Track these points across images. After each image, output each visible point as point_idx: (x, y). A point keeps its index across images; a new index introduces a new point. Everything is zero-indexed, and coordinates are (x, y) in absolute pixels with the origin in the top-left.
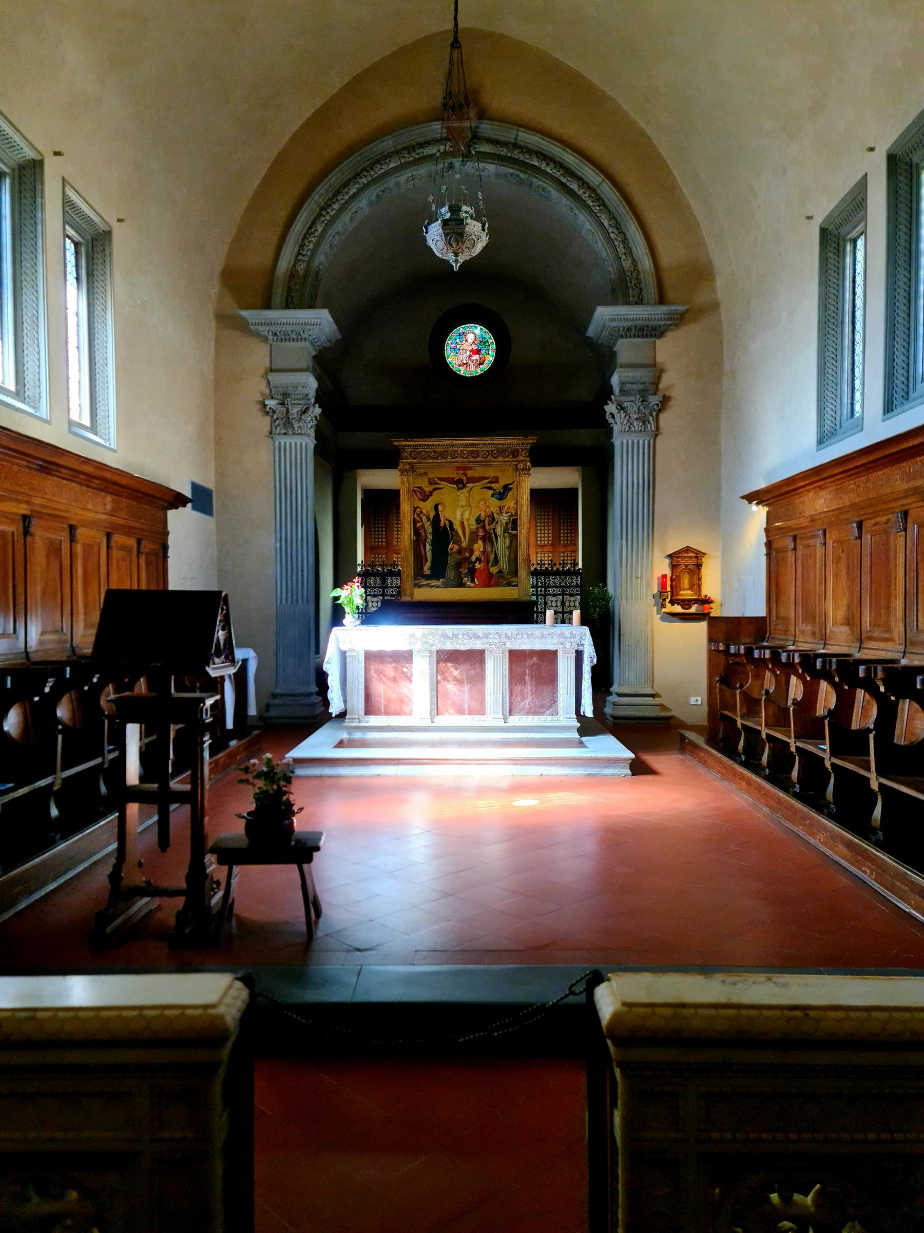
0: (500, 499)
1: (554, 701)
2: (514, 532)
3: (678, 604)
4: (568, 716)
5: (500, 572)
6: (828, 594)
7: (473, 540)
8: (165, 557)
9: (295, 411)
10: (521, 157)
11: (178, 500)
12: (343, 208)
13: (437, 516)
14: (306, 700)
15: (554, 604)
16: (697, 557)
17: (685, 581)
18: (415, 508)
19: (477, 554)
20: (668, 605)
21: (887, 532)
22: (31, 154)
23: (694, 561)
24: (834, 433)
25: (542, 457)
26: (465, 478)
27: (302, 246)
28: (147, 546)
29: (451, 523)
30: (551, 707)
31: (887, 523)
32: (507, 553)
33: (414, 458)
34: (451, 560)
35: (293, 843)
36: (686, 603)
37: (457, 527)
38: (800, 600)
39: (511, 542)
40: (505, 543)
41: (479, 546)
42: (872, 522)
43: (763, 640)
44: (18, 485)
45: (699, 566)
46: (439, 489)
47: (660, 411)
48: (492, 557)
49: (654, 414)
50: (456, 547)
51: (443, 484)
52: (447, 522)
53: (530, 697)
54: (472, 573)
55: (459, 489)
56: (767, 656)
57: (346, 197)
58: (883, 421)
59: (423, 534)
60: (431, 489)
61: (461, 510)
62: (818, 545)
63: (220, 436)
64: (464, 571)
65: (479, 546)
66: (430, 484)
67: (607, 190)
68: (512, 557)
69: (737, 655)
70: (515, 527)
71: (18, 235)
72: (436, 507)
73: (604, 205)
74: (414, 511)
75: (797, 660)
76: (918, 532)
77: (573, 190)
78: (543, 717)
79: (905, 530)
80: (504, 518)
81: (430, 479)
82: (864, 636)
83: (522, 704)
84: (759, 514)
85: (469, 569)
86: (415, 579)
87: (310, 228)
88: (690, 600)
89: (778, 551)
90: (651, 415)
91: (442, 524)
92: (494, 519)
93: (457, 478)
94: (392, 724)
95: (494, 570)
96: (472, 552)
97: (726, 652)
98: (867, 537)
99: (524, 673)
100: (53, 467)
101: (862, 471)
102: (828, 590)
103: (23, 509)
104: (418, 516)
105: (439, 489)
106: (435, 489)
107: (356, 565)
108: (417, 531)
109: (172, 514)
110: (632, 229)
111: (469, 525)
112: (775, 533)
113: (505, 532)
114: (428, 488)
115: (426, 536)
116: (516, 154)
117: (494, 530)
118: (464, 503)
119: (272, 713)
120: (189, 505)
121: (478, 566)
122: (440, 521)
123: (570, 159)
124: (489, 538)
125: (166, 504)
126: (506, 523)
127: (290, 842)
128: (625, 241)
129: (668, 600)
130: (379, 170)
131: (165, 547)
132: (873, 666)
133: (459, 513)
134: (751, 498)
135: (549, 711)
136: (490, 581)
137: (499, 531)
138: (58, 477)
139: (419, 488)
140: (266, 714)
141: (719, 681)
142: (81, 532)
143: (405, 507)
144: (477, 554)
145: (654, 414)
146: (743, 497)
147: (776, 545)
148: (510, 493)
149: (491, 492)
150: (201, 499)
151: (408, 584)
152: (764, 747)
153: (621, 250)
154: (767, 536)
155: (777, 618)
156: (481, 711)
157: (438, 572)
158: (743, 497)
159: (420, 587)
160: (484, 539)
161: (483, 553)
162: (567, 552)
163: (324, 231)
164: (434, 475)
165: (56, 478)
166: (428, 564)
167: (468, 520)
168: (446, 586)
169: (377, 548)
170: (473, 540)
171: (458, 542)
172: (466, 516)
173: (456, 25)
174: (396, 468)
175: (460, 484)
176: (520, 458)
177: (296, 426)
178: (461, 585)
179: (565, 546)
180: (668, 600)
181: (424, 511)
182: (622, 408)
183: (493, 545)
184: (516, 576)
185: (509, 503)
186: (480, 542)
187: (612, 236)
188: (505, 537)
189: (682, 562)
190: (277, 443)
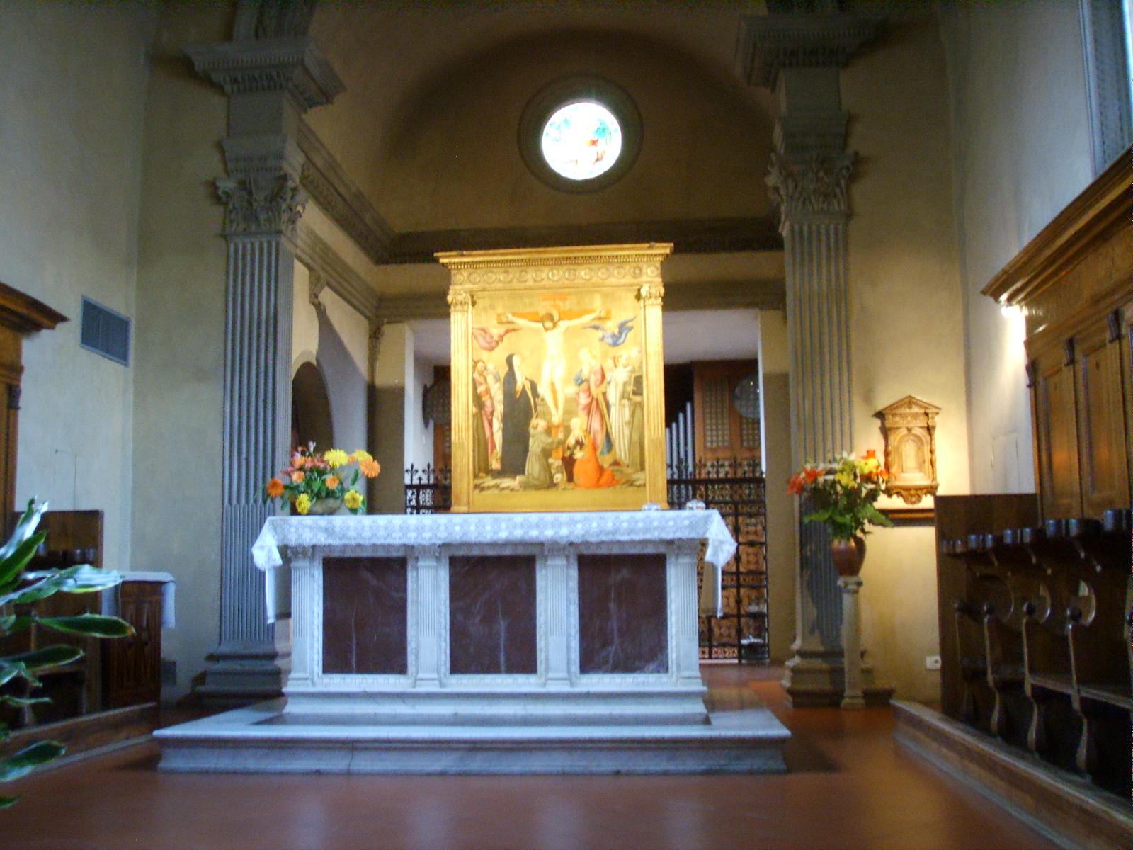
2: (638, 399)
4: (686, 674)
7: (569, 413)
9: (260, 196)
13: (510, 377)
16: (926, 414)
23: (922, 422)
29: (534, 387)
32: (627, 432)
33: (474, 284)
34: (535, 445)
36: (912, 492)
37: (543, 390)
39: (633, 415)
40: (623, 416)
45: (930, 430)
46: (514, 330)
48: (600, 439)
49: (843, 182)
51: (521, 322)
53: (617, 641)
54: (569, 463)
55: (546, 329)
56: (1027, 539)
59: (488, 403)
64: (556, 462)
66: (500, 323)
68: (636, 437)
70: (638, 391)
72: (509, 361)
74: (474, 368)
75: (1074, 530)
83: (604, 653)
85: (563, 459)
86: (476, 476)
90: (838, 185)
91: (519, 387)
92: (603, 377)
93: (542, 312)
94: (370, 689)
95: (606, 461)
96: (568, 431)
104: (481, 374)
105: (514, 330)
106: (507, 332)
113: (623, 397)
114: (496, 331)
115: (493, 406)
117: (604, 394)
121: (579, 455)
124: (598, 407)
126: (625, 384)
135: (652, 666)
137: (613, 397)
140: (200, 688)
141: (961, 609)
145: (843, 182)
148: (630, 334)
156: (525, 662)
158: (984, 293)
159: (483, 489)
161: (588, 431)
168: (526, 486)
171: (546, 415)
173: (1081, 489)
177: (262, 217)
178: (552, 485)
181: (490, 367)
185: (628, 352)
188: (622, 406)
190: (232, 247)
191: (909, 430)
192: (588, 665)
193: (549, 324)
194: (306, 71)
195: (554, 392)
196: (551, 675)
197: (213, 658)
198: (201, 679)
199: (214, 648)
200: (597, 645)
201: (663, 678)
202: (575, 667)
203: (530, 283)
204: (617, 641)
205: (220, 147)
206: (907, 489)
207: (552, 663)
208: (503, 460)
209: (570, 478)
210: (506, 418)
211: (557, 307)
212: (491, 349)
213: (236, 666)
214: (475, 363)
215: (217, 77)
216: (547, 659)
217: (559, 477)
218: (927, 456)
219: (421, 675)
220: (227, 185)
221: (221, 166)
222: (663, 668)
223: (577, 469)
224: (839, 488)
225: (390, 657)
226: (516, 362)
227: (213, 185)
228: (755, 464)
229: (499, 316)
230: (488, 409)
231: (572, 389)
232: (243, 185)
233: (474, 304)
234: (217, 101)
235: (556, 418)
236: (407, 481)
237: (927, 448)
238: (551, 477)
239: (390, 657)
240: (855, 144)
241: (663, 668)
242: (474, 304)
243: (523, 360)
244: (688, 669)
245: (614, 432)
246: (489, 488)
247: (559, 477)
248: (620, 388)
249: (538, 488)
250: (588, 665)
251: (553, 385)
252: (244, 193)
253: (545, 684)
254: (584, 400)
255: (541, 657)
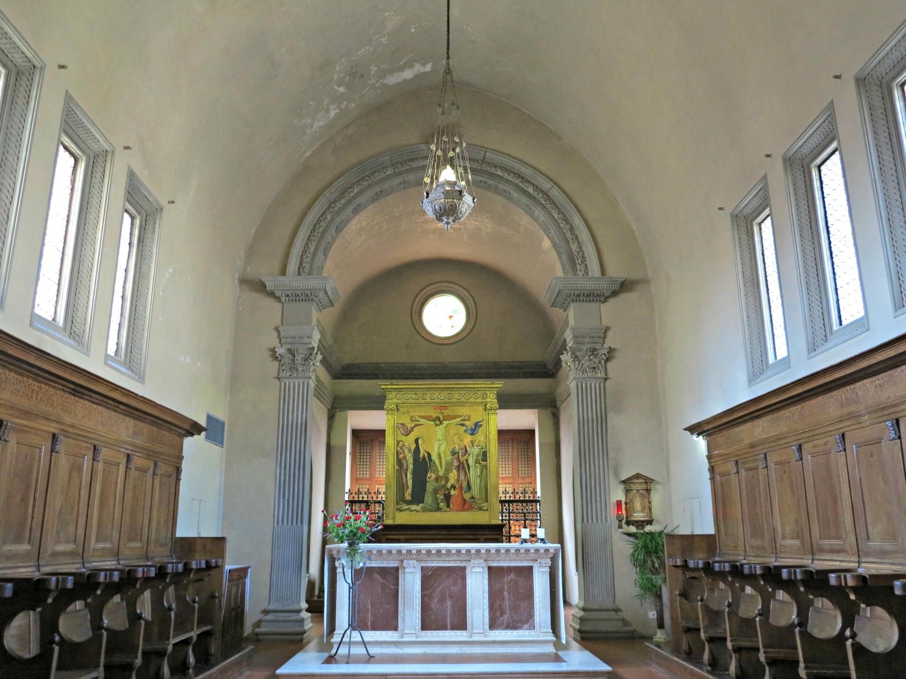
0: (472, 434)
1: (531, 616)
2: (484, 463)
3: (633, 525)
4: (544, 630)
5: (473, 498)
6: (774, 511)
7: (448, 470)
8: (178, 479)
9: (299, 358)
10: (488, 169)
11: (194, 429)
12: (349, 202)
13: (417, 449)
14: (294, 617)
15: (517, 528)
17: (638, 504)
18: (398, 442)
19: (452, 481)
20: (624, 526)
21: (827, 453)
22: (106, 146)
23: (644, 486)
24: (762, 371)
25: (506, 401)
26: (441, 417)
27: (313, 230)
28: (163, 468)
29: (429, 455)
30: (527, 622)
31: (825, 445)
32: (478, 481)
34: (430, 487)
35: (811, 597)
37: (434, 457)
38: (747, 519)
39: (481, 472)
41: (453, 476)
42: (811, 444)
43: (714, 556)
44: (52, 406)
45: (648, 491)
47: (607, 360)
48: (465, 484)
50: (434, 476)
51: (423, 421)
52: (426, 455)
53: (508, 612)
54: (448, 498)
55: (437, 425)
57: (352, 195)
58: (809, 359)
60: (412, 425)
61: (438, 444)
62: (760, 467)
63: (235, 381)
64: (440, 497)
65: (453, 476)
67: (555, 193)
68: (483, 484)
69: (696, 569)
70: (485, 458)
71: (84, 213)
72: (417, 441)
73: (554, 204)
75: (759, 572)
76: (857, 451)
77: (529, 193)
78: (520, 632)
79: (845, 450)
80: (476, 451)
81: (411, 417)
82: (815, 547)
83: (501, 619)
84: (701, 443)
86: (397, 504)
87: (322, 216)
88: (643, 522)
89: (723, 475)
92: (466, 451)
93: (435, 415)
95: (467, 496)
96: (447, 480)
97: (685, 566)
98: (807, 458)
99: (503, 589)
100: (86, 392)
101: (796, 402)
102: (774, 507)
103: (53, 428)
106: (416, 426)
107: (344, 493)
108: (399, 462)
109: (188, 442)
110: (577, 221)
111: (445, 456)
112: (717, 459)
113: (476, 463)
114: (410, 425)
116: (484, 167)
117: (467, 460)
118: (440, 437)
119: (263, 629)
120: (203, 434)
121: (453, 492)
122: (419, 453)
123: (526, 171)
124: (462, 467)
125: (183, 432)
127: (812, 594)
128: (572, 229)
129: (624, 521)
130: (378, 176)
131: (178, 470)
132: (842, 575)
133: (436, 446)
134: (695, 429)
135: (526, 626)
136: (466, 506)
137: (471, 462)
138: (89, 401)
139: (403, 424)
140: (257, 630)
141: (680, 595)
142: (104, 453)
143: (390, 440)
144: (452, 481)
145: (603, 362)
146: (685, 429)
147: (717, 470)
149: (464, 428)
150: (213, 430)
151: (391, 507)
152: (731, 658)
153: (569, 235)
154: (710, 462)
155: (726, 535)
156: (461, 624)
157: (418, 497)
158: (685, 429)
159: (401, 511)
160: (458, 468)
161: (458, 480)
162: (524, 483)
163: (332, 218)
164: (416, 413)
165: (87, 402)
166: (410, 490)
167: (444, 452)
168: (424, 510)
169: (363, 479)
170: (448, 470)
171: (436, 471)
172: (443, 448)
174: (383, 409)
175: (438, 421)
176: (489, 400)
177: (300, 369)
178: (439, 509)
179: (523, 478)
180: (624, 521)
181: (406, 444)
182: (576, 357)
183: (466, 473)
184: (487, 501)
185: (480, 437)
186: (455, 471)
187: (562, 225)
188: (476, 467)
189: (634, 487)
191: (638, 491)
192: (493, 626)
193: (438, 423)
194: (326, 292)
195: (440, 458)
196: (475, 631)
197: (266, 612)
198: (258, 624)
199: (265, 606)
200: (498, 614)
201: (533, 632)
202: (487, 627)
203: (428, 400)
204: (508, 612)
205: (277, 329)
206: (637, 522)
207: (476, 624)
208: (413, 495)
209: (448, 506)
210: (414, 473)
211: (442, 413)
212: (407, 435)
213: (280, 616)
214: (398, 442)
215: (278, 294)
216: (472, 622)
217: (442, 505)
218: (647, 504)
219: (406, 631)
220: (280, 351)
221: (278, 340)
222: (533, 627)
223: (451, 501)
224: (334, 356)
225: (390, 622)
226: (420, 441)
227: (273, 351)
228: (534, 492)
229: (411, 417)
230: (405, 467)
231: (450, 458)
232: (290, 351)
233: (398, 410)
234: (277, 306)
235: (441, 474)
236: (347, 499)
237: (646, 500)
238: (438, 504)
239: (390, 622)
240: (609, 343)
241: (533, 627)
242: (398, 410)
243: (424, 442)
244: (545, 628)
245: (472, 480)
246: (404, 510)
247: (442, 505)
248: (475, 457)
249: (431, 511)
250: (493, 626)
251: (440, 455)
252: (290, 356)
253: (471, 636)
254: (456, 463)
255: (469, 621)
